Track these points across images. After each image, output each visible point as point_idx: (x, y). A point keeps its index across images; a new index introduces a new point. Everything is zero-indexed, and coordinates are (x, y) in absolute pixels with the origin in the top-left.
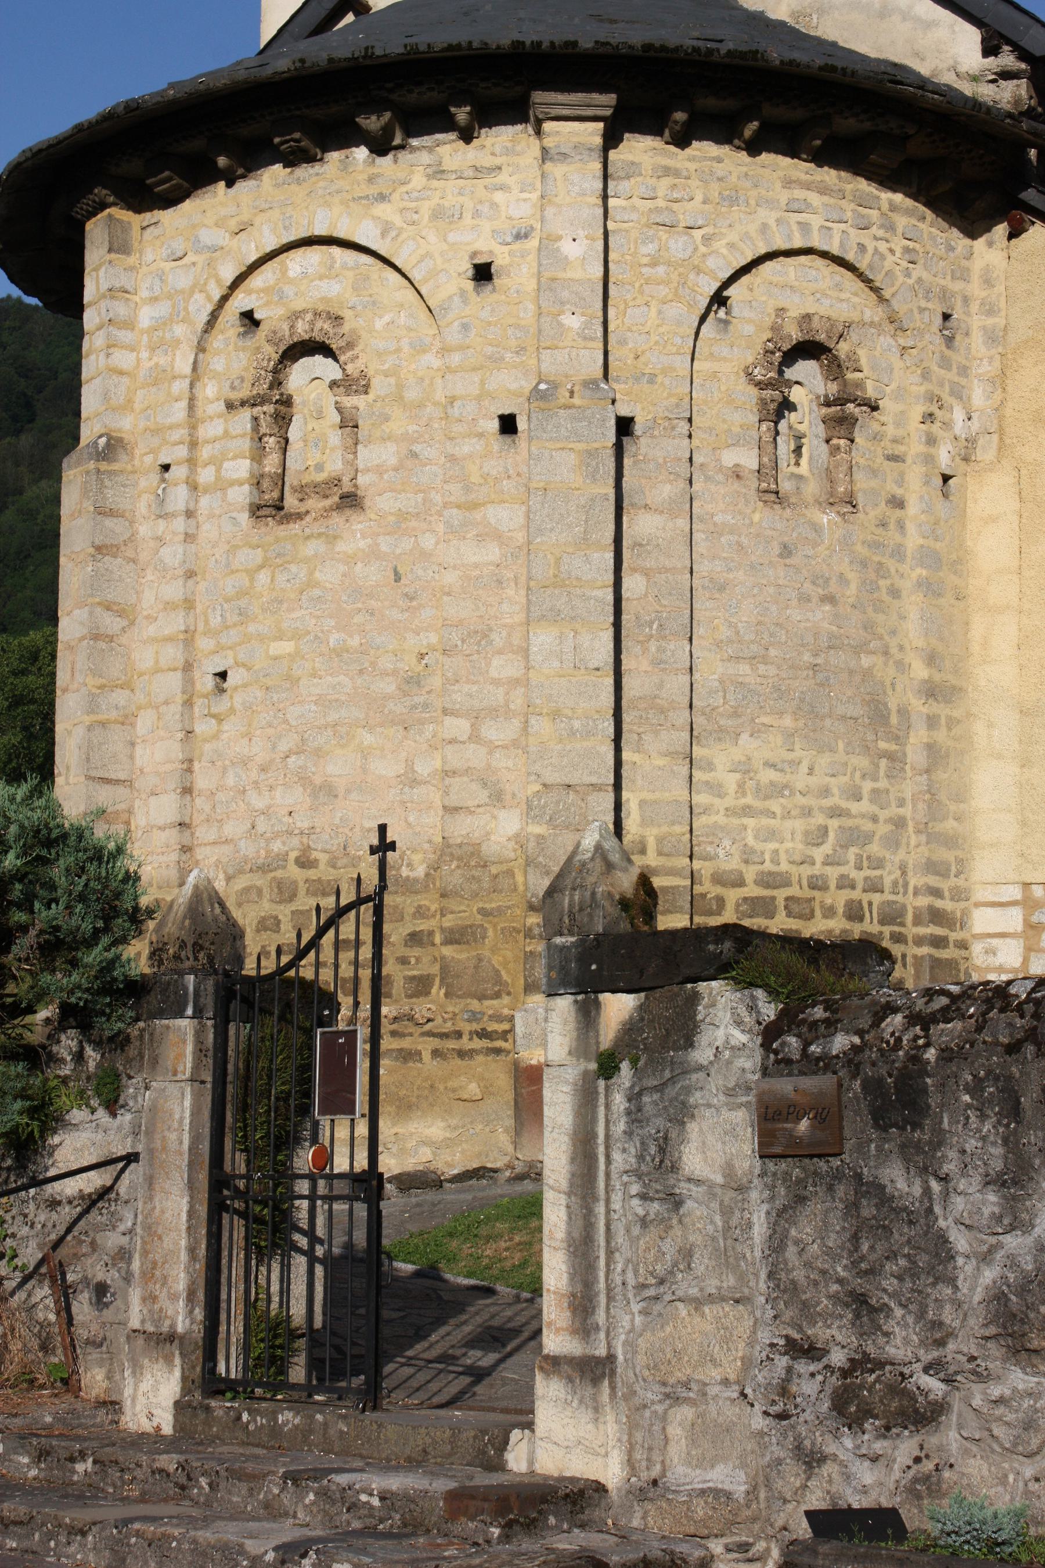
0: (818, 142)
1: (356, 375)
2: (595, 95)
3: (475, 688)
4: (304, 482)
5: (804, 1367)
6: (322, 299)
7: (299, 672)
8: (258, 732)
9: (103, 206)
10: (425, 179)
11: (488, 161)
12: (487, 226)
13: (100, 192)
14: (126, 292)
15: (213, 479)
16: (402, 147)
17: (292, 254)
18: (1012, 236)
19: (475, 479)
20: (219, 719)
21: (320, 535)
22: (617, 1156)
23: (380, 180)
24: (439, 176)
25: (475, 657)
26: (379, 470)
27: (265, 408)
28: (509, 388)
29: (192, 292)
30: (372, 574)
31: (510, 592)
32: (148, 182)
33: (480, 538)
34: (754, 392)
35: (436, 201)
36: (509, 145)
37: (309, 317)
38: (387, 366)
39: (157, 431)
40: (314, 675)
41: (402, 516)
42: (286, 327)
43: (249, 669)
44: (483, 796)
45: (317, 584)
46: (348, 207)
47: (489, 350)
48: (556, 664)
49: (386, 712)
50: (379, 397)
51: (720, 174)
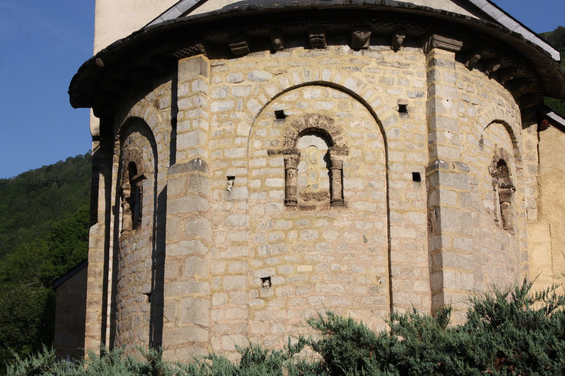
0: (512, 78)
1: (341, 146)
2: (455, 41)
3: (407, 295)
4: (307, 192)
6: (322, 110)
7: (315, 281)
8: (291, 308)
9: (199, 52)
10: (376, 64)
11: (404, 61)
12: (404, 89)
13: (200, 46)
14: (205, 94)
15: (259, 186)
16: (366, 48)
17: (306, 88)
18: (539, 130)
19: (403, 199)
20: (266, 300)
21: (325, 217)
23: (356, 61)
24: (383, 64)
25: (407, 280)
26: (355, 190)
27: (292, 156)
29: (248, 98)
30: (353, 238)
31: (421, 252)
32: (231, 45)
33: (407, 227)
34: (490, 177)
35: (381, 74)
36: (413, 56)
37: (316, 117)
38: (357, 144)
40: (323, 282)
41: (367, 213)
42: (303, 120)
43: (285, 277)
45: (324, 240)
46: (340, 71)
47: (407, 143)
48: (454, 287)
49: (362, 302)
50: (353, 157)
51: (482, 84)
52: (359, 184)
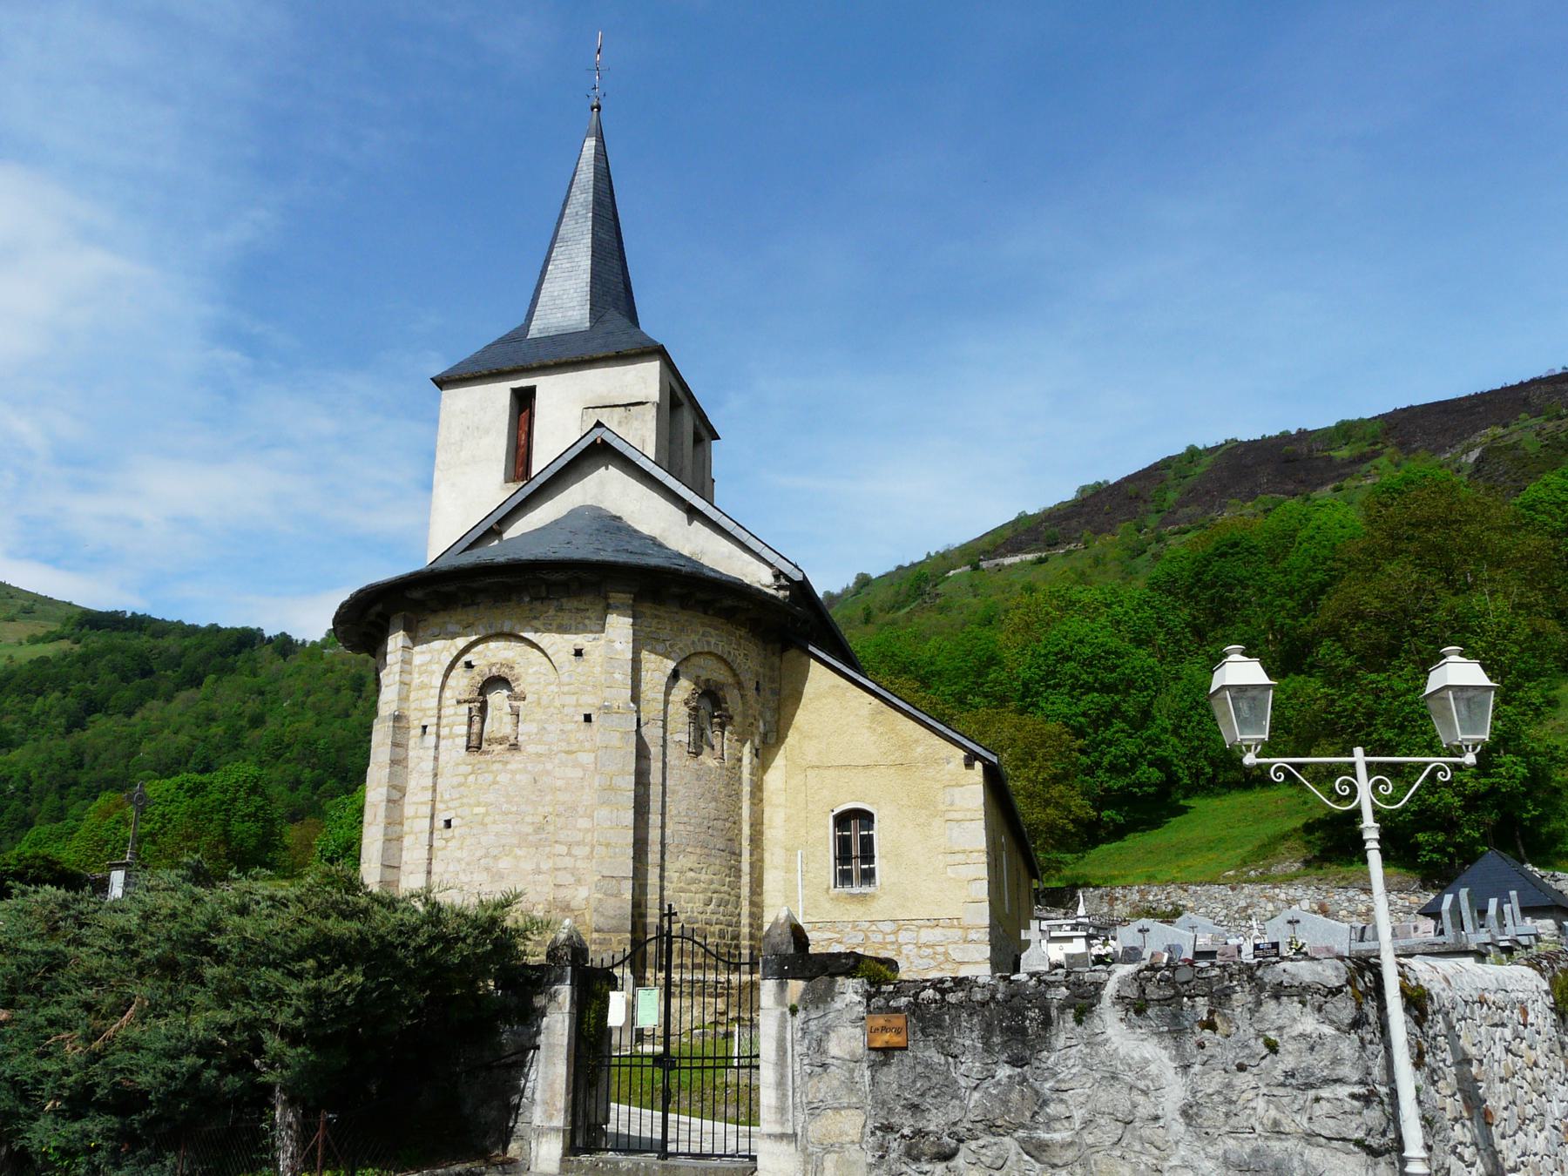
5: (890, 1137)
20: (447, 841)
22: (797, 1048)
28: (589, 703)
30: (522, 779)
39: (423, 710)
40: (494, 822)
41: (540, 755)
44: (572, 880)
52: (533, 728)
